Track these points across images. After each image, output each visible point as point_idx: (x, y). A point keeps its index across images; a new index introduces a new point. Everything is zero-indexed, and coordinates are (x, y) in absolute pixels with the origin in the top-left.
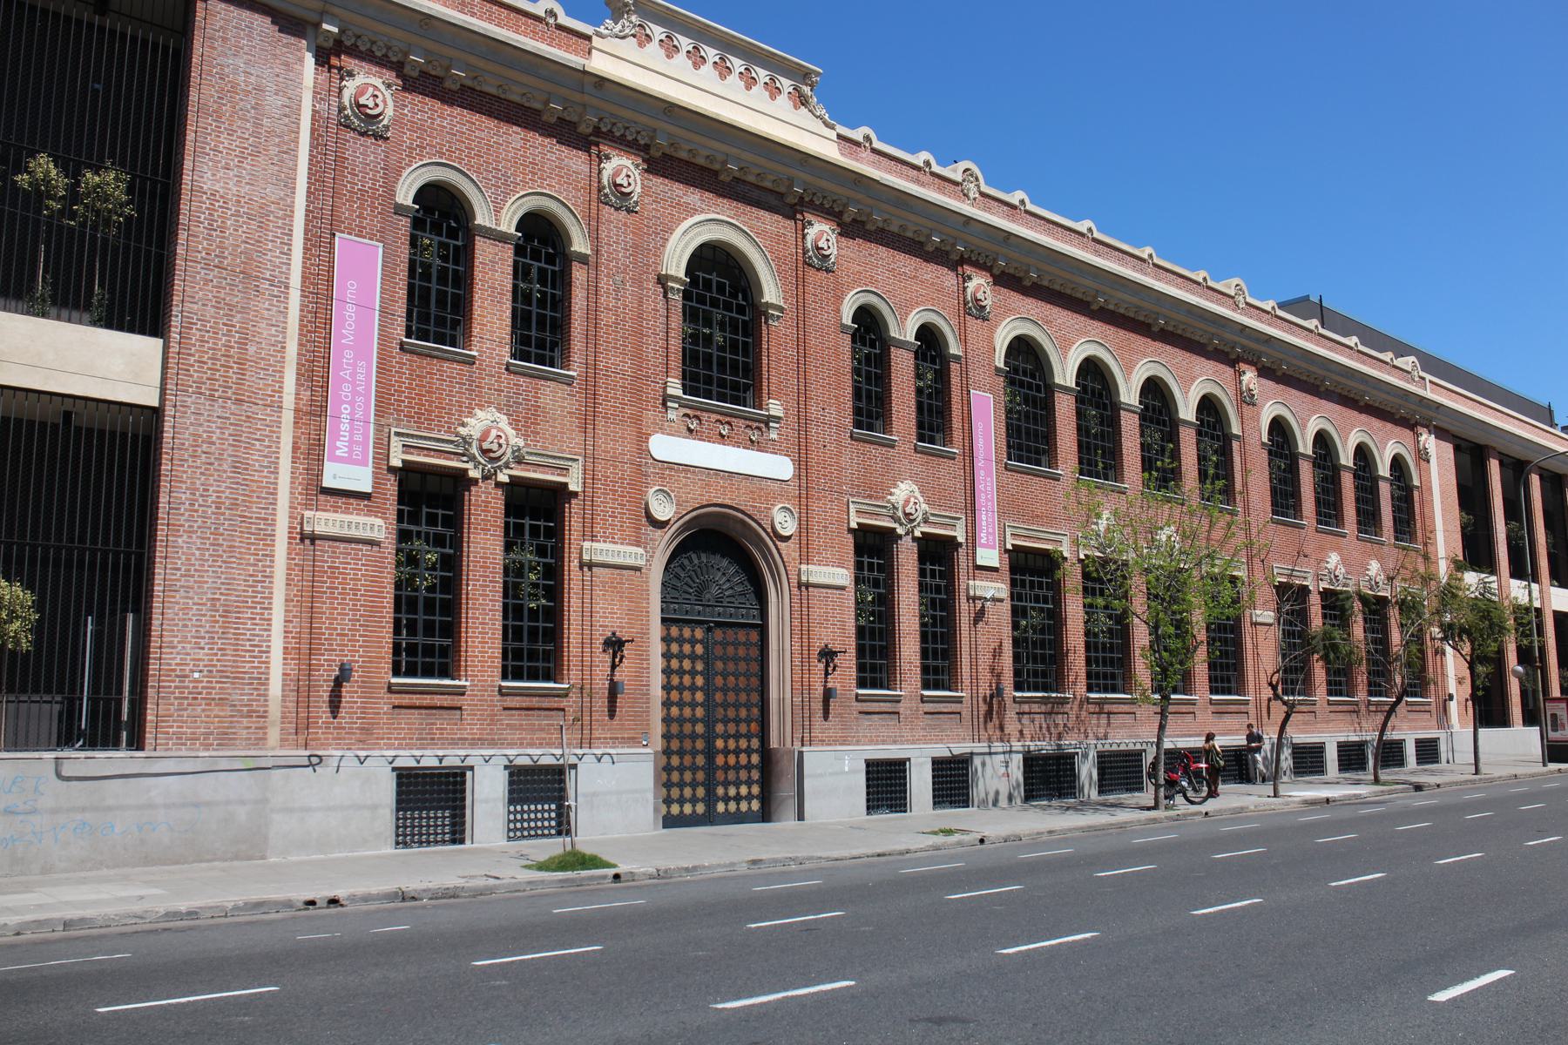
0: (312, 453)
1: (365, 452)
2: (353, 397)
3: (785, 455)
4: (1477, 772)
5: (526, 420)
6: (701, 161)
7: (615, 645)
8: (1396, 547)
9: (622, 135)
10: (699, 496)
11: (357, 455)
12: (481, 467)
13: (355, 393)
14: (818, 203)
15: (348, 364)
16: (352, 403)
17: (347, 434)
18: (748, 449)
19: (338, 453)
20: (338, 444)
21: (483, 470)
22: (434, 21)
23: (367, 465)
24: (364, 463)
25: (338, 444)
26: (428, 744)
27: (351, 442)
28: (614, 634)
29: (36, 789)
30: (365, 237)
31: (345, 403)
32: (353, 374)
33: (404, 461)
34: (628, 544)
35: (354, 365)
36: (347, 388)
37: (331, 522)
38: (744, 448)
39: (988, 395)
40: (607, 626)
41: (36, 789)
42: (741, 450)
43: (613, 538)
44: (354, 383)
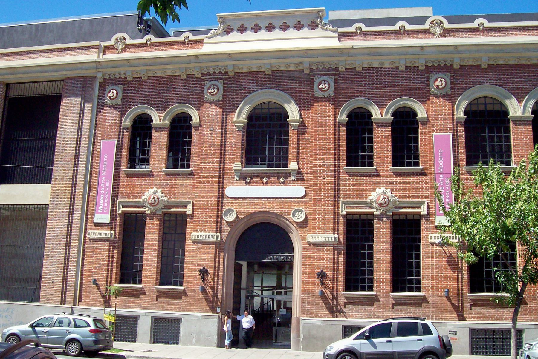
0: (88, 213)
1: (108, 210)
2: (105, 192)
3: (301, 185)
4: (20, 340)
5: (170, 190)
6: (254, 70)
7: (204, 272)
8: (397, 174)
9: (214, 72)
10: (247, 209)
11: (105, 211)
12: (379, 211)
13: (105, 191)
14: (123, 77)
15: (103, 182)
16: (104, 194)
17: (102, 204)
18: (279, 186)
19: (99, 211)
20: (99, 208)
21: (380, 211)
22: (130, 61)
23: (108, 214)
24: (107, 213)
25: (99, 208)
26: (127, 307)
27: (104, 207)
28: (204, 268)
29: (12, 312)
30: (439, 133)
31: (102, 194)
32: (444, 183)
33: (346, 212)
34: (211, 232)
35: (105, 182)
36: (103, 189)
37: (313, 238)
38: (276, 186)
39: (449, 133)
40: (201, 265)
41: (12, 312)
42: (275, 186)
43: (205, 230)
44: (105, 188)
